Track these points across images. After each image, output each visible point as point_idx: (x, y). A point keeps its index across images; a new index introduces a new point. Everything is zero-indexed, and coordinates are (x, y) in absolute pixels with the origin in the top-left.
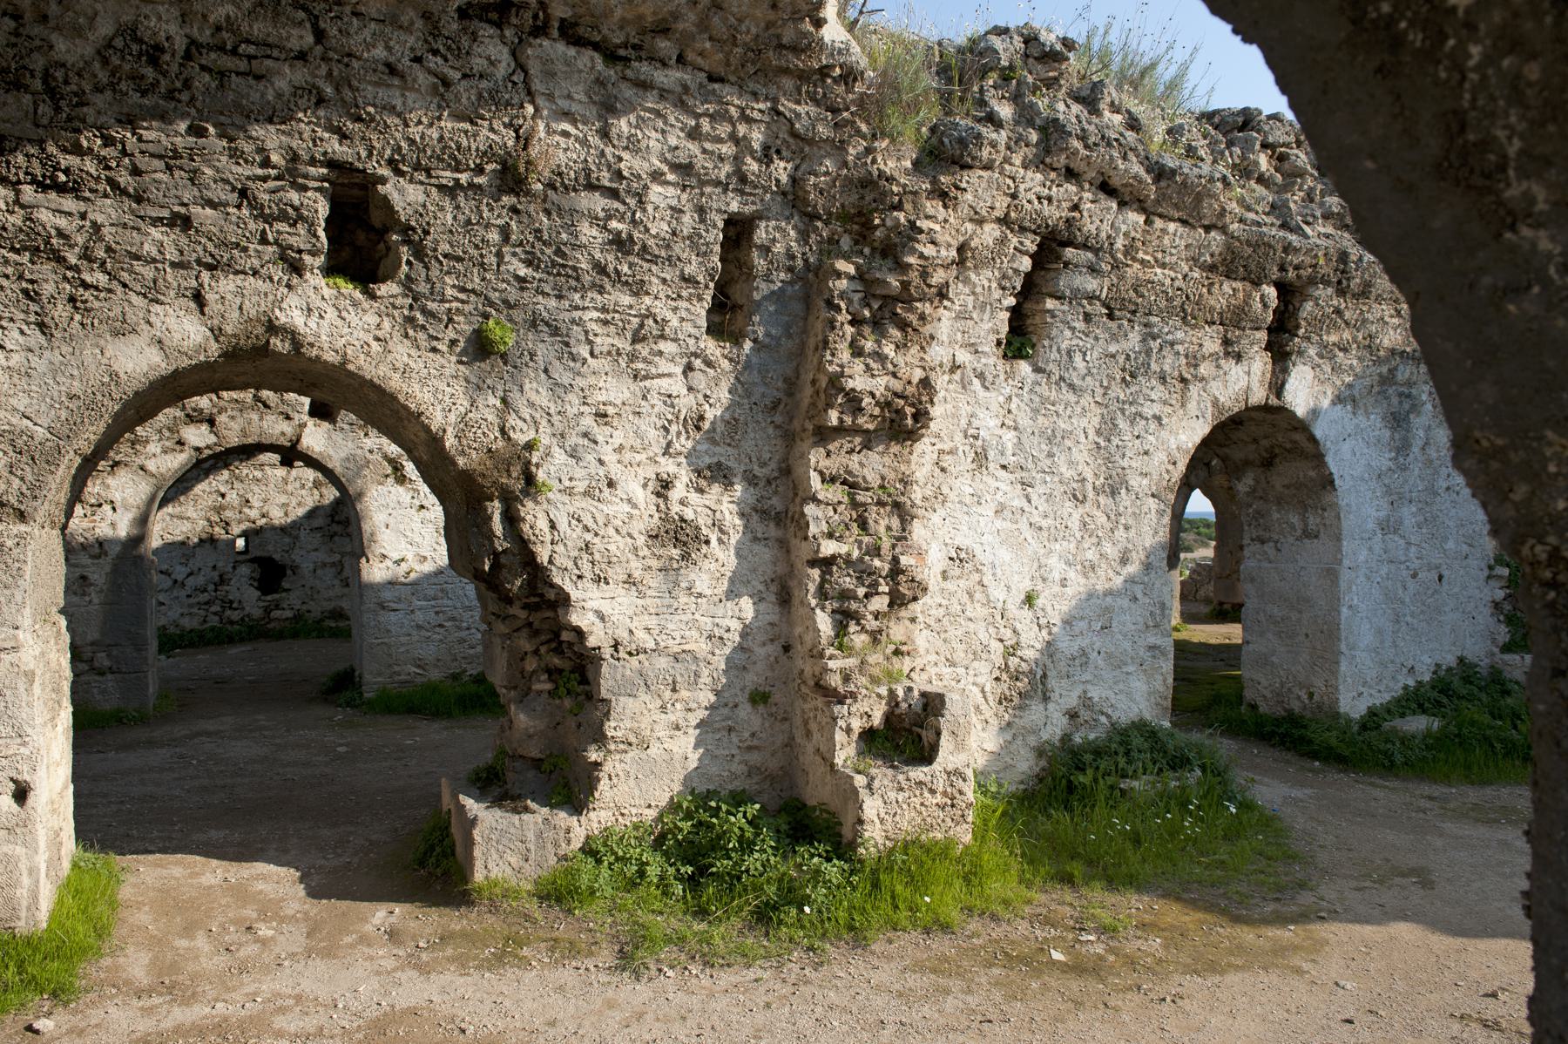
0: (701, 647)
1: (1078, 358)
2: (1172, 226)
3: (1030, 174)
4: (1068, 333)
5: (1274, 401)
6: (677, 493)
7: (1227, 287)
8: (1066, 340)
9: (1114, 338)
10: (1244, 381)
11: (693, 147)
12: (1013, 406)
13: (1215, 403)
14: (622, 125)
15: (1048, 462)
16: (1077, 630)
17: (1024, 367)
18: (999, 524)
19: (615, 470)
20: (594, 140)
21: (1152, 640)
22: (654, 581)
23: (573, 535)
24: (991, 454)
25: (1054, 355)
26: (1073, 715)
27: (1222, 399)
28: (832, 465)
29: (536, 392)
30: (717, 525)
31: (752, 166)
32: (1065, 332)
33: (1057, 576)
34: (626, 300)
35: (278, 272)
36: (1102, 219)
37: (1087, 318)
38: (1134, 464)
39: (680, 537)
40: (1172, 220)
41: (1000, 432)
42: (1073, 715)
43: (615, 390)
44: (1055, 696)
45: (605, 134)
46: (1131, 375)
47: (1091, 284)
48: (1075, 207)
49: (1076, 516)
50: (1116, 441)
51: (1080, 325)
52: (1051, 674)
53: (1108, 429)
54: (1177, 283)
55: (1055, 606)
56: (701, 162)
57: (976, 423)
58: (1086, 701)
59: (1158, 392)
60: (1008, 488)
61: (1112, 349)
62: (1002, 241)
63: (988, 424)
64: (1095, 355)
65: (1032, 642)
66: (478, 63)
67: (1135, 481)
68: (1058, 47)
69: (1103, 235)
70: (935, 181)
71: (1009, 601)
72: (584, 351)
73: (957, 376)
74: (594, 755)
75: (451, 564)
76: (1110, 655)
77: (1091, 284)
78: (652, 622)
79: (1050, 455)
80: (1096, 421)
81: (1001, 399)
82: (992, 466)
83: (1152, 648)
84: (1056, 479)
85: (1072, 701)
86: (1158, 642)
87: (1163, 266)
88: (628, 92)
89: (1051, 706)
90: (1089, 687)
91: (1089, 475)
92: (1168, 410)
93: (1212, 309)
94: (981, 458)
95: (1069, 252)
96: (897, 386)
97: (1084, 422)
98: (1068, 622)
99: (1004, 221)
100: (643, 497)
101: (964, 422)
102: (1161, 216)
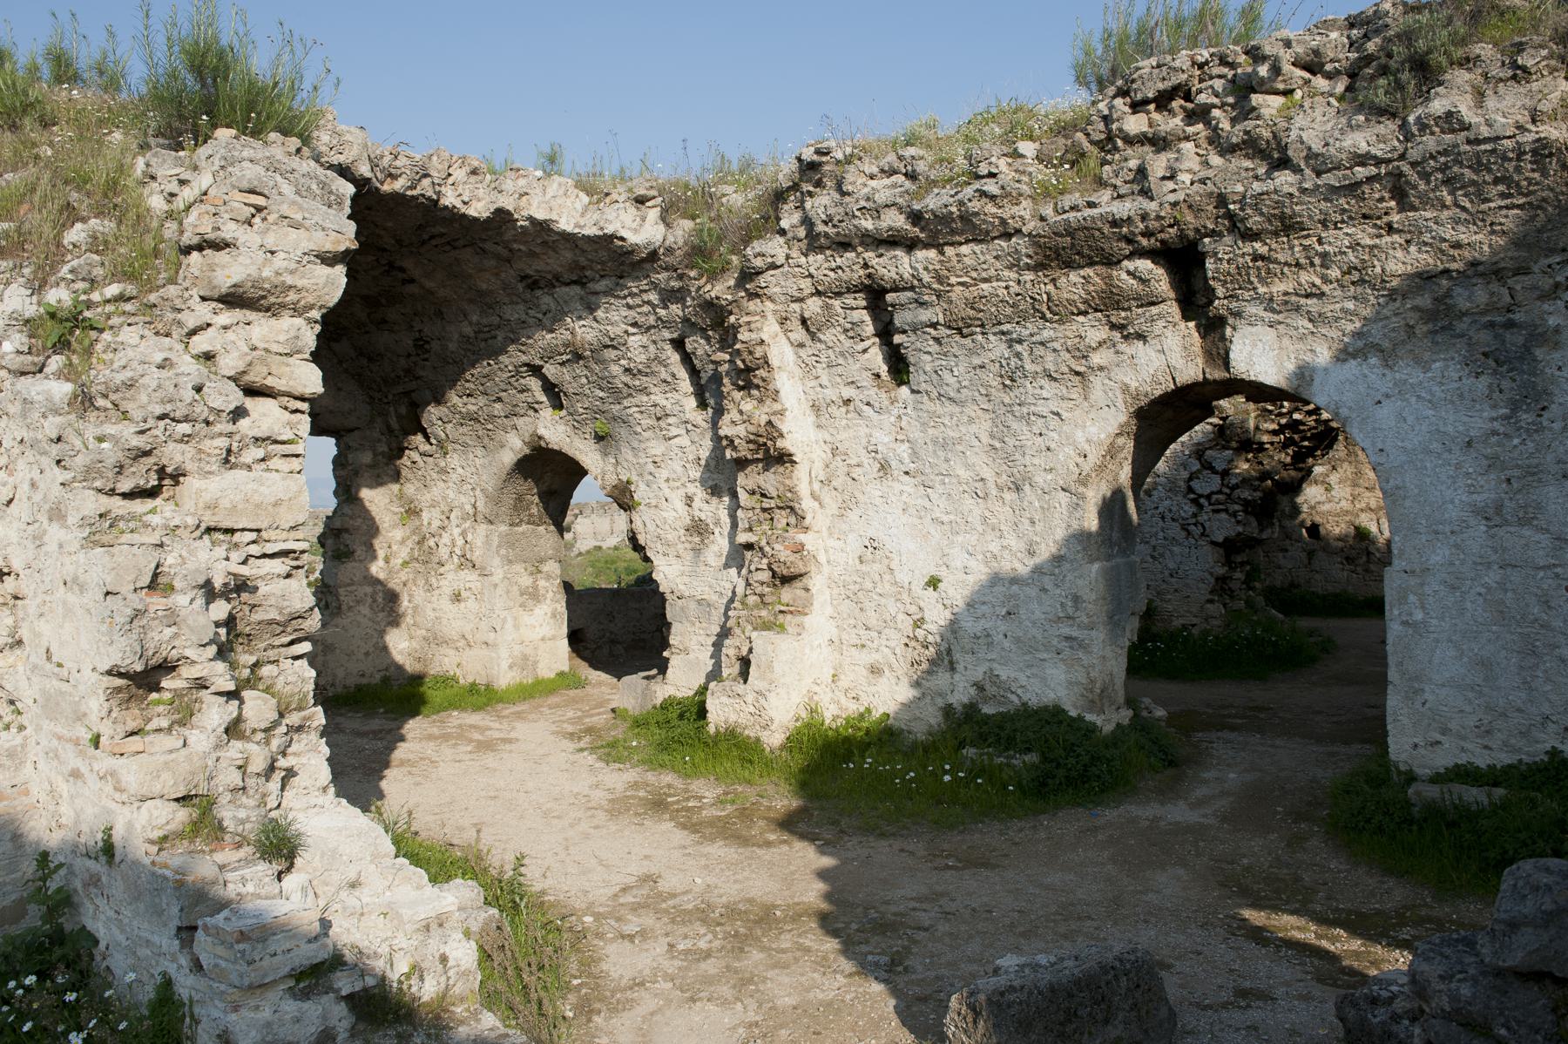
0: (714, 597)
1: (946, 375)
2: (964, 249)
3: (811, 258)
4: (927, 358)
5: (1217, 374)
6: (697, 503)
7: (1074, 277)
8: (927, 362)
9: (971, 352)
10: (1169, 354)
11: (632, 313)
12: (903, 424)
13: (1125, 389)
14: (600, 314)
15: (945, 466)
16: (979, 613)
17: (904, 390)
18: (904, 519)
19: (667, 492)
20: (595, 325)
21: (1066, 631)
22: (689, 556)
23: (651, 527)
24: (894, 464)
25: (922, 378)
26: (980, 687)
27: (1134, 384)
28: (751, 485)
29: (626, 453)
30: (717, 523)
31: (662, 312)
32: (922, 353)
33: (959, 564)
34: (645, 398)
35: (531, 412)
36: (895, 265)
37: (937, 340)
38: (1036, 461)
39: (698, 529)
40: (961, 244)
41: (893, 445)
42: (980, 687)
43: (657, 448)
44: (960, 667)
45: (595, 319)
46: (1010, 379)
47: (925, 315)
48: (866, 266)
49: (977, 511)
50: (1011, 441)
51: (934, 348)
52: (955, 648)
53: (1000, 433)
54: (1012, 290)
55: (957, 591)
56: (641, 320)
57: (873, 441)
58: (993, 677)
59: (1049, 389)
60: (911, 490)
61: (977, 361)
62: (827, 307)
63: (883, 439)
64: (961, 369)
65: (937, 618)
66: (544, 308)
67: (1041, 479)
68: (815, 158)
69: (906, 276)
70: (746, 290)
71: (915, 583)
72: (639, 429)
73: (851, 408)
74: (665, 654)
75: (1098, 534)
76: (1018, 640)
77: (925, 315)
78: (687, 579)
79: (947, 460)
80: (987, 425)
81: (893, 419)
82: (896, 473)
83: (1068, 638)
84: (954, 480)
85: (978, 674)
86: (1074, 634)
87: (986, 280)
88: (593, 299)
89: (957, 677)
90: (995, 665)
91: (987, 473)
92: (1065, 404)
93: (1071, 302)
94: (884, 467)
95: (890, 297)
96: (752, 429)
97: (973, 428)
98: (970, 605)
99: (818, 293)
100: (679, 505)
101: (864, 441)
102: (952, 244)
